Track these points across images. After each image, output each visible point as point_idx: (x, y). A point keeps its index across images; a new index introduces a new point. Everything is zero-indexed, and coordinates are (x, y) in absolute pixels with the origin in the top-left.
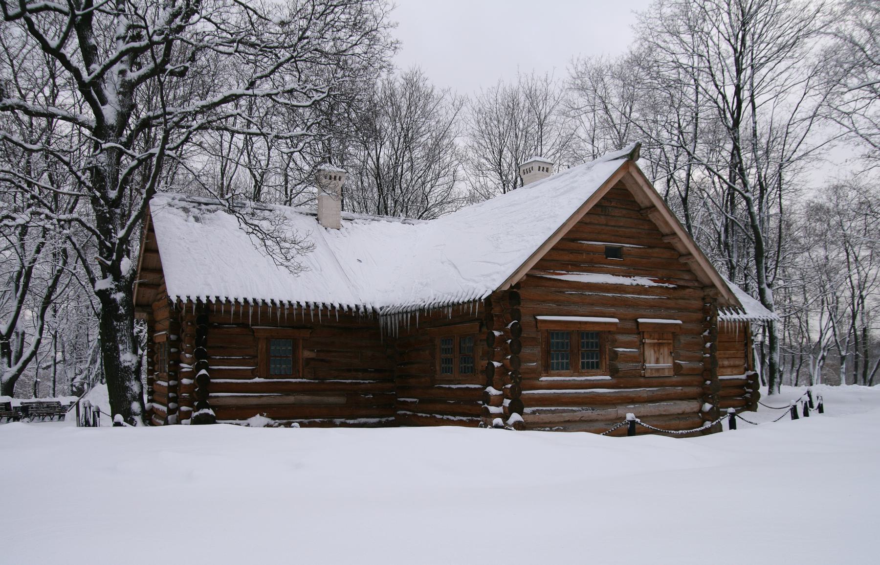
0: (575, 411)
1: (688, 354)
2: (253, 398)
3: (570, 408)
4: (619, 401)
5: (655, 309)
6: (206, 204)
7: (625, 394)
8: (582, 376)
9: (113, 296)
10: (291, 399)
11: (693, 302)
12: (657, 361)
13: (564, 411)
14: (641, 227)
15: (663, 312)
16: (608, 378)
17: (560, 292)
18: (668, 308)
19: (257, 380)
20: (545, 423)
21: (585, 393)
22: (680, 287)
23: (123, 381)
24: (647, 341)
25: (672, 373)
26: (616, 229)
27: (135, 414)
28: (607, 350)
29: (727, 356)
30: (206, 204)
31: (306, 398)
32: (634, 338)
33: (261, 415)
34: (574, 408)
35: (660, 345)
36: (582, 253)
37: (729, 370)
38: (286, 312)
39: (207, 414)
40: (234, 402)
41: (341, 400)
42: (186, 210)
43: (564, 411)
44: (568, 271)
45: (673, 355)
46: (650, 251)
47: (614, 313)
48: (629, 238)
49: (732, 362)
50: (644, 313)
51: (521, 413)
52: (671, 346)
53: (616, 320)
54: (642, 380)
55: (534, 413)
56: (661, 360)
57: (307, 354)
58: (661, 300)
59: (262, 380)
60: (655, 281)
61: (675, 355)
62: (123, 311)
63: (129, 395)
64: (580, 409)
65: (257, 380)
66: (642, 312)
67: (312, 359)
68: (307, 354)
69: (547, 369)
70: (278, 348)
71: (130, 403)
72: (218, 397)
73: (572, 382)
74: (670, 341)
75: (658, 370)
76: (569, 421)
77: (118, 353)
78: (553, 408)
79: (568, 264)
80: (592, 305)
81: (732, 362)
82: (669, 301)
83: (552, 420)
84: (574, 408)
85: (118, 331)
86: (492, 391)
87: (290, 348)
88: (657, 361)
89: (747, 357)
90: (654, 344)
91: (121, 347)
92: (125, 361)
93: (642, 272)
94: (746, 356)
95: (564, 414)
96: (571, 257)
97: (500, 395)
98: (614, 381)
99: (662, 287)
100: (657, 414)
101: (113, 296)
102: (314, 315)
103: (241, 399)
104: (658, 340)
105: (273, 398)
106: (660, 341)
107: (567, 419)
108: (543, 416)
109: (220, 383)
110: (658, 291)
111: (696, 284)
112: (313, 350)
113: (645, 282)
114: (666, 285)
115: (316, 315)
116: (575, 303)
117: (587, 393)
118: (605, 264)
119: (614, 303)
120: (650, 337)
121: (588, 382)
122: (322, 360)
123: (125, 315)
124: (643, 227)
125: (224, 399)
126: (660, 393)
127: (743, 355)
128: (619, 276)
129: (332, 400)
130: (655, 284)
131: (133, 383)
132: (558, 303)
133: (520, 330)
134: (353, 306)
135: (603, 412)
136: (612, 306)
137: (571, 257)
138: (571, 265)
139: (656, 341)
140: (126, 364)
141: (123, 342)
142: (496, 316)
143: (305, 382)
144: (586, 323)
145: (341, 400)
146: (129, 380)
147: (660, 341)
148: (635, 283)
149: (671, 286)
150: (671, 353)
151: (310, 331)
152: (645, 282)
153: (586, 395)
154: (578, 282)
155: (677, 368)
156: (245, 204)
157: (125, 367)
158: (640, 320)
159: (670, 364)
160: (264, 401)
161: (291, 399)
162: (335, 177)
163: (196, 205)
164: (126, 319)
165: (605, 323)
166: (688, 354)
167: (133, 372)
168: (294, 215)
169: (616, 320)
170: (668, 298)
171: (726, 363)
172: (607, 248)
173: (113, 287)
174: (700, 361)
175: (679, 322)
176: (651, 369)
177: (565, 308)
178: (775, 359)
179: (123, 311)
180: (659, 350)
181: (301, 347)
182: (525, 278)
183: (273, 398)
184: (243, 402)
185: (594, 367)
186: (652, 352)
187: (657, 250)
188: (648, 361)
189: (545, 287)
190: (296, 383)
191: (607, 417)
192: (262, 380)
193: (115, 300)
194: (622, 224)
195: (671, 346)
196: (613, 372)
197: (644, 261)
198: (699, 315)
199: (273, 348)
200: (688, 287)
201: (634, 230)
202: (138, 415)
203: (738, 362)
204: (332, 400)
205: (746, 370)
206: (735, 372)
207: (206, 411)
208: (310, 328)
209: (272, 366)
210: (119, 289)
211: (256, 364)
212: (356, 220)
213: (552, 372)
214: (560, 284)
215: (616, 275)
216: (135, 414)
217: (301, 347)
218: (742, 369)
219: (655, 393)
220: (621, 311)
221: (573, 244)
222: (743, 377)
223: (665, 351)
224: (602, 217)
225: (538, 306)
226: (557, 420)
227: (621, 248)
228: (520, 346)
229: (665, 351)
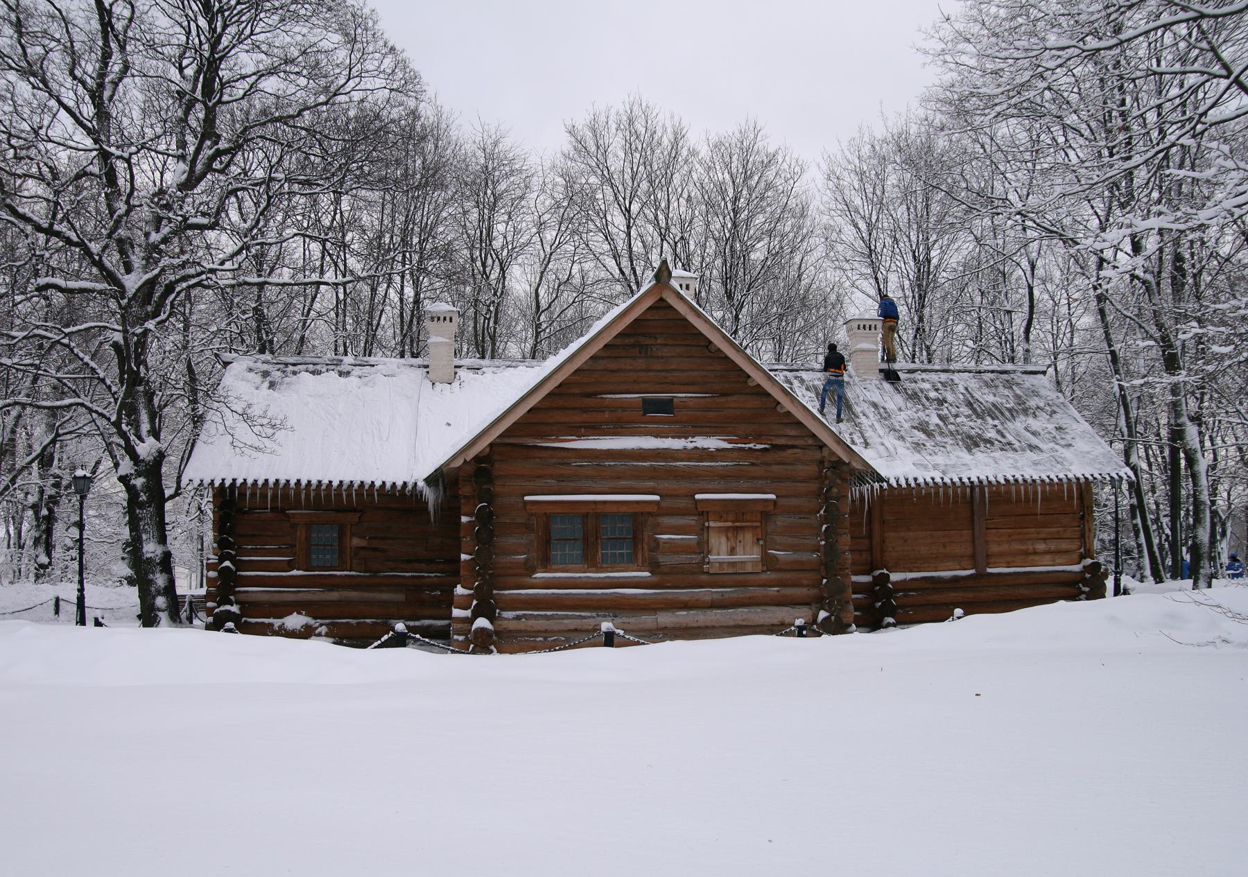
0: (585, 618)
1: (790, 540)
2: (288, 594)
3: (578, 614)
4: (660, 606)
5: (727, 480)
6: (294, 365)
7: (670, 597)
8: (602, 572)
9: (133, 482)
10: (334, 596)
11: (800, 467)
12: (732, 551)
13: (567, 617)
14: (709, 368)
15: (743, 484)
16: (647, 574)
17: (563, 464)
18: (754, 478)
19: (295, 572)
20: (539, 631)
21: (602, 594)
22: (776, 447)
23: (146, 574)
24: (712, 524)
25: (759, 568)
26: (664, 374)
27: (159, 610)
28: (646, 537)
29: (1043, 536)
30: (294, 365)
31: (354, 595)
32: (690, 521)
33: (299, 613)
34: (583, 614)
35: (736, 529)
36: (603, 411)
37: (1048, 557)
38: (312, 494)
39: (229, 611)
40: (265, 597)
41: (400, 597)
42: (266, 374)
43: (567, 617)
44: (580, 436)
45: (761, 542)
46: (722, 400)
47: (653, 488)
48: (686, 385)
49: (1052, 546)
50: (710, 486)
51: (492, 619)
52: (759, 531)
53: (657, 498)
54: (704, 577)
55: (518, 618)
56: (739, 549)
57: (356, 542)
58: (737, 468)
59: (301, 573)
60: (730, 442)
61: (765, 541)
62: (145, 498)
63: (153, 589)
64: (594, 614)
65: (295, 572)
66: (697, 486)
67: (363, 548)
68: (356, 542)
69: (546, 564)
70: (320, 535)
71: (154, 598)
72: (247, 592)
73: (584, 580)
74: (755, 524)
75: (733, 564)
76: (576, 630)
77: (141, 544)
78: (549, 613)
79: (581, 427)
80: (619, 478)
81: (1052, 546)
82: (752, 468)
83: (549, 628)
84: (583, 614)
85: (141, 519)
86: (459, 590)
87: (335, 535)
88: (732, 551)
89: (1084, 537)
90: (727, 529)
91: (144, 537)
92: (147, 552)
93: (708, 430)
94: (1083, 536)
95: (565, 621)
96: (585, 417)
97: (469, 595)
98: (655, 579)
99: (740, 449)
100: (732, 623)
101: (133, 482)
102: (347, 495)
103: (288, 595)
104: (733, 522)
105: (314, 594)
106: (737, 524)
107: (573, 627)
108: (532, 622)
109: (251, 576)
110: (735, 454)
111: (810, 442)
112: (364, 537)
113: (712, 443)
114: (751, 445)
115: (308, 495)
116: (587, 477)
117: (606, 594)
118: (645, 423)
119: (654, 474)
120: (720, 519)
121: (610, 580)
122: (375, 549)
123: (146, 502)
124: (713, 368)
125: (254, 595)
126: (735, 595)
127: (1077, 535)
128: (667, 437)
129: (386, 596)
130: (730, 446)
131: (158, 575)
132: (561, 478)
133: (491, 514)
134: (399, 484)
135: (632, 620)
136: (652, 478)
137: (585, 417)
138: (585, 427)
139: (730, 524)
140: (149, 555)
141: (146, 531)
142: (465, 497)
143: (353, 576)
144: (605, 502)
145: (400, 597)
146: (153, 573)
147: (737, 524)
148: (690, 446)
149: (759, 447)
150: (758, 540)
151: (359, 514)
152: (712, 443)
153: (605, 597)
154: (608, 450)
155: (768, 562)
156: (341, 361)
157: (147, 559)
158: (698, 496)
159: (756, 556)
160: (309, 597)
161: (334, 596)
162: (445, 319)
163: (281, 366)
164: (150, 506)
165: (638, 502)
166: (790, 540)
167: (158, 564)
168: (403, 369)
169: (657, 498)
170: (753, 464)
171: (1041, 546)
172: (644, 400)
173: (133, 472)
174: (814, 551)
175: (773, 496)
176: (721, 563)
177: (570, 484)
178: (1200, 537)
179: (145, 498)
180: (736, 537)
181: (348, 533)
182: (488, 450)
183: (314, 594)
184: (277, 598)
185: (631, 561)
186: (723, 539)
187: (734, 398)
188: (715, 551)
189: (540, 458)
190: (341, 576)
191: (641, 626)
192: (301, 573)
193: (134, 486)
194: (674, 367)
195: (759, 531)
196: (654, 567)
197: (711, 415)
198: (814, 486)
199: (314, 535)
200: (793, 447)
201: (695, 373)
202: (163, 611)
203: (1064, 545)
204: (386, 596)
205: (1082, 557)
206: (1058, 561)
207: (228, 607)
208: (359, 511)
209: (314, 556)
210: (139, 474)
211: (294, 554)
212: (484, 369)
213: (554, 567)
214: (563, 454)
215: (661, 437)
216: (159, 610)
217: (348, 533)
218: (1075, 556)
219: (726, 596)
220: (665, 485)
221: (589, 400)
222: (1077, 568)
223: (748, 537)
224: (640, 360)
225: (527, 483)
226: (556, 628)
227: (671, 401)
228: (491, 534)
229: (748, 537)
